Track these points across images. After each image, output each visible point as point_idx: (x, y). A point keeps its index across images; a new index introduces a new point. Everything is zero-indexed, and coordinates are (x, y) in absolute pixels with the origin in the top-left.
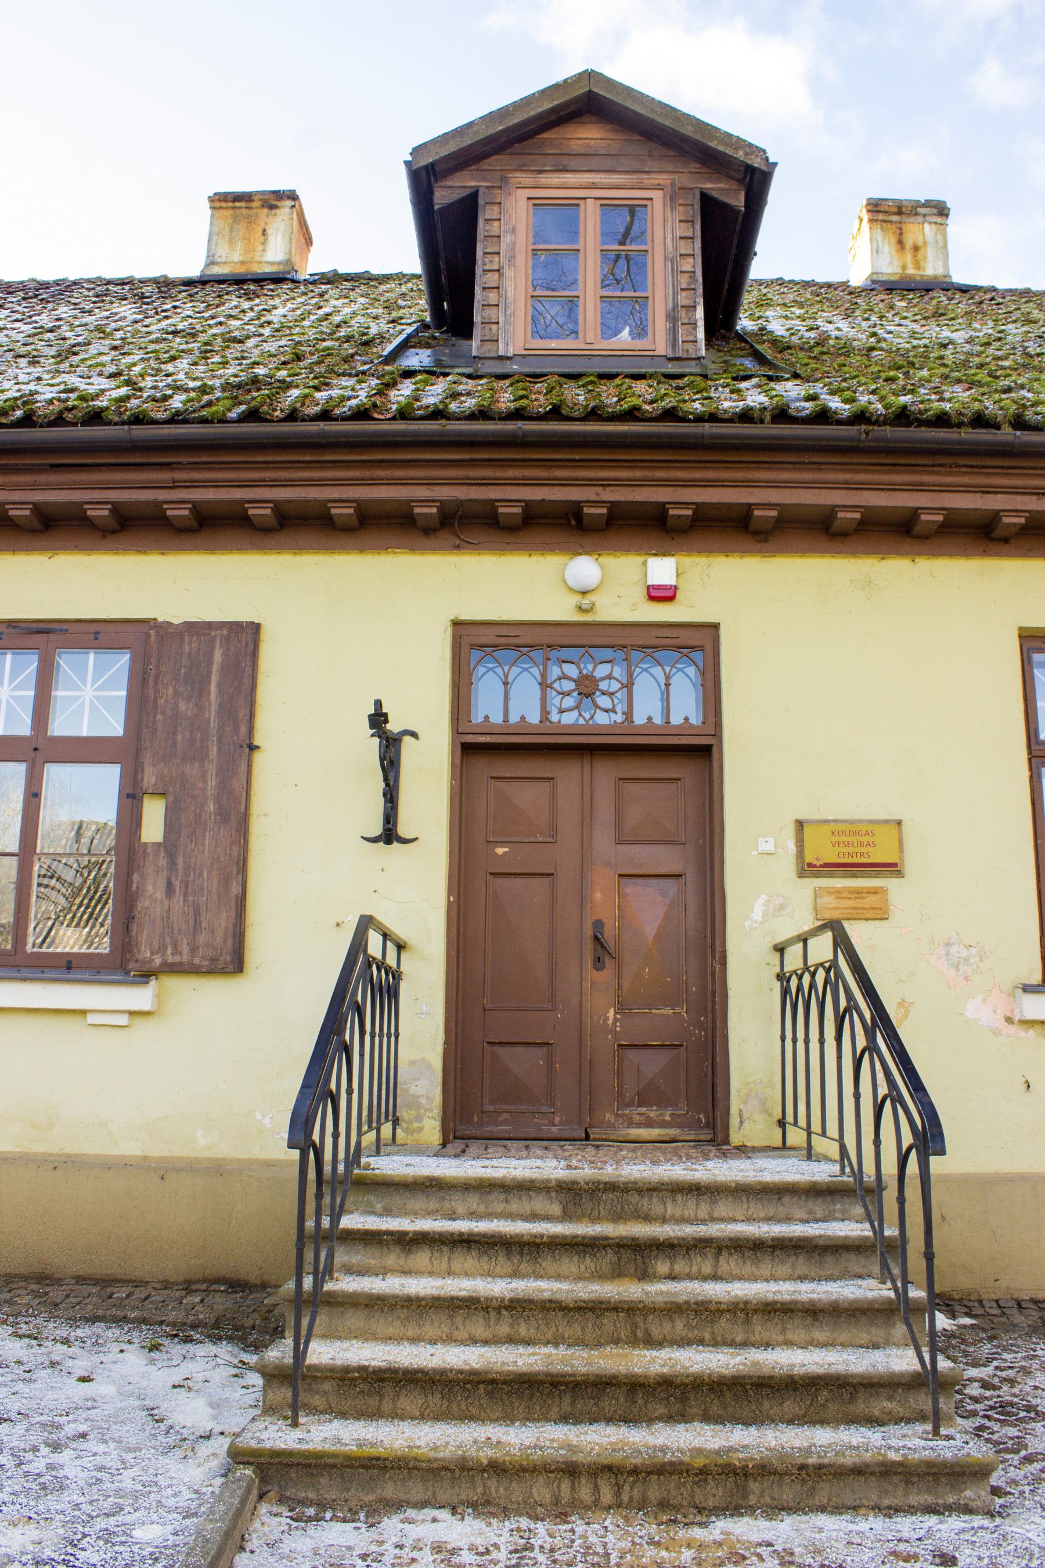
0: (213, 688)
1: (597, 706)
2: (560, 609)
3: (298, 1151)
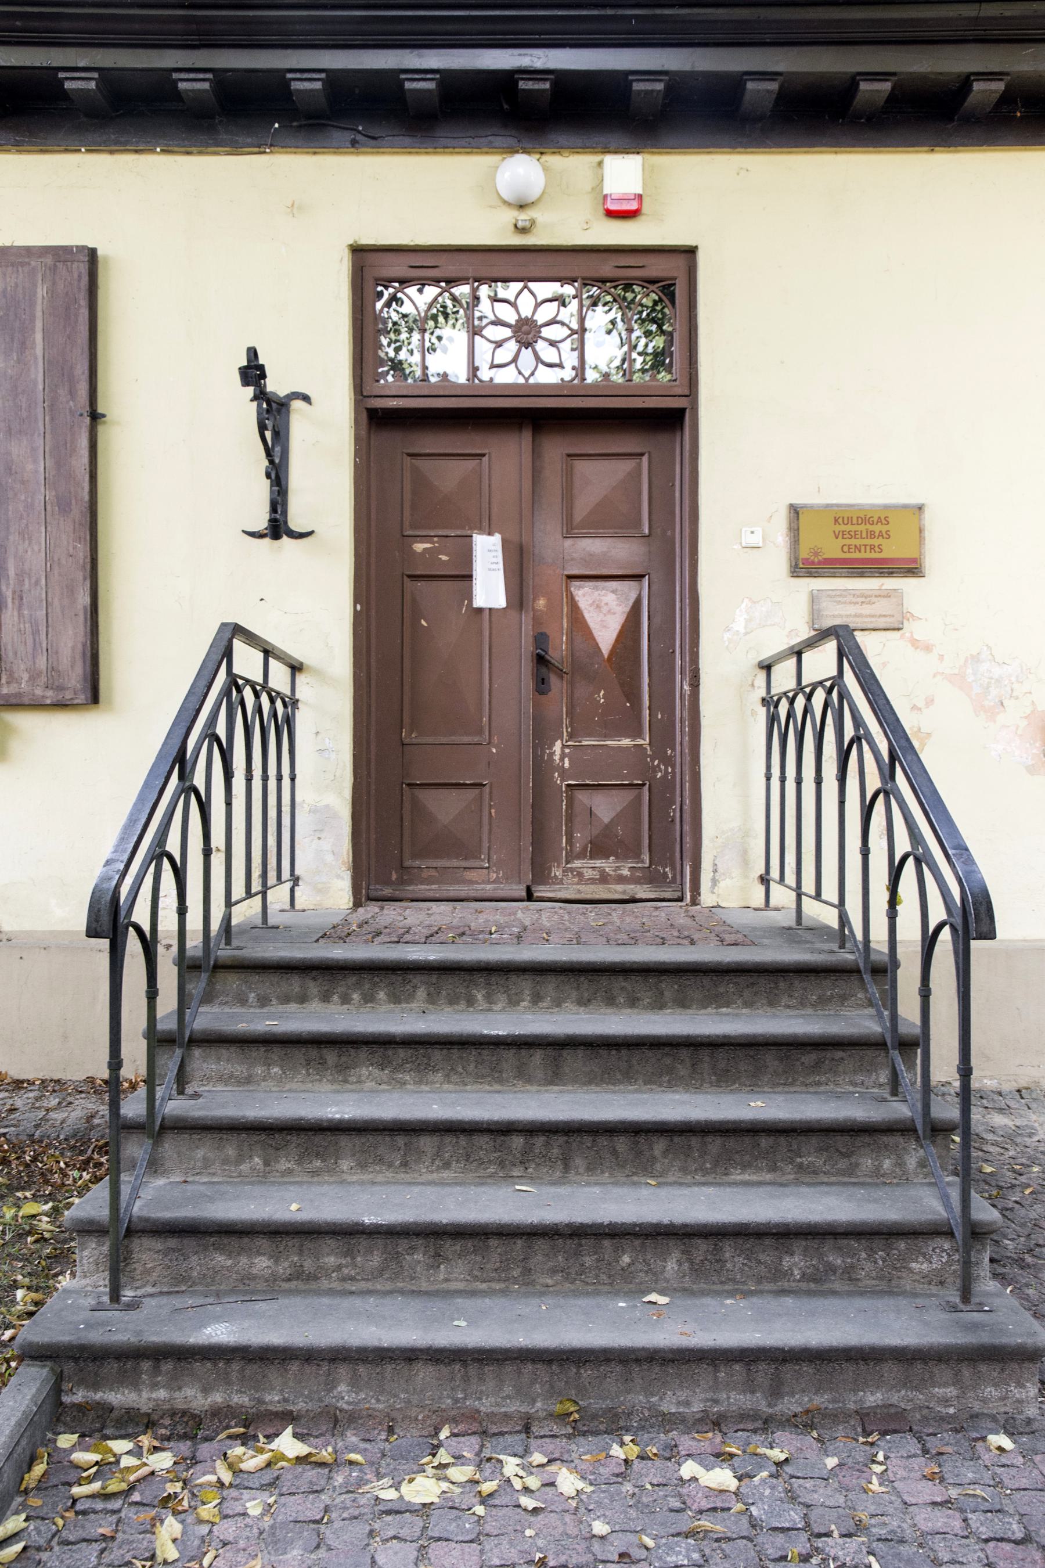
0: (39, 337)
1: (538, 359)
2: (491, 229)
3: (108, 941)
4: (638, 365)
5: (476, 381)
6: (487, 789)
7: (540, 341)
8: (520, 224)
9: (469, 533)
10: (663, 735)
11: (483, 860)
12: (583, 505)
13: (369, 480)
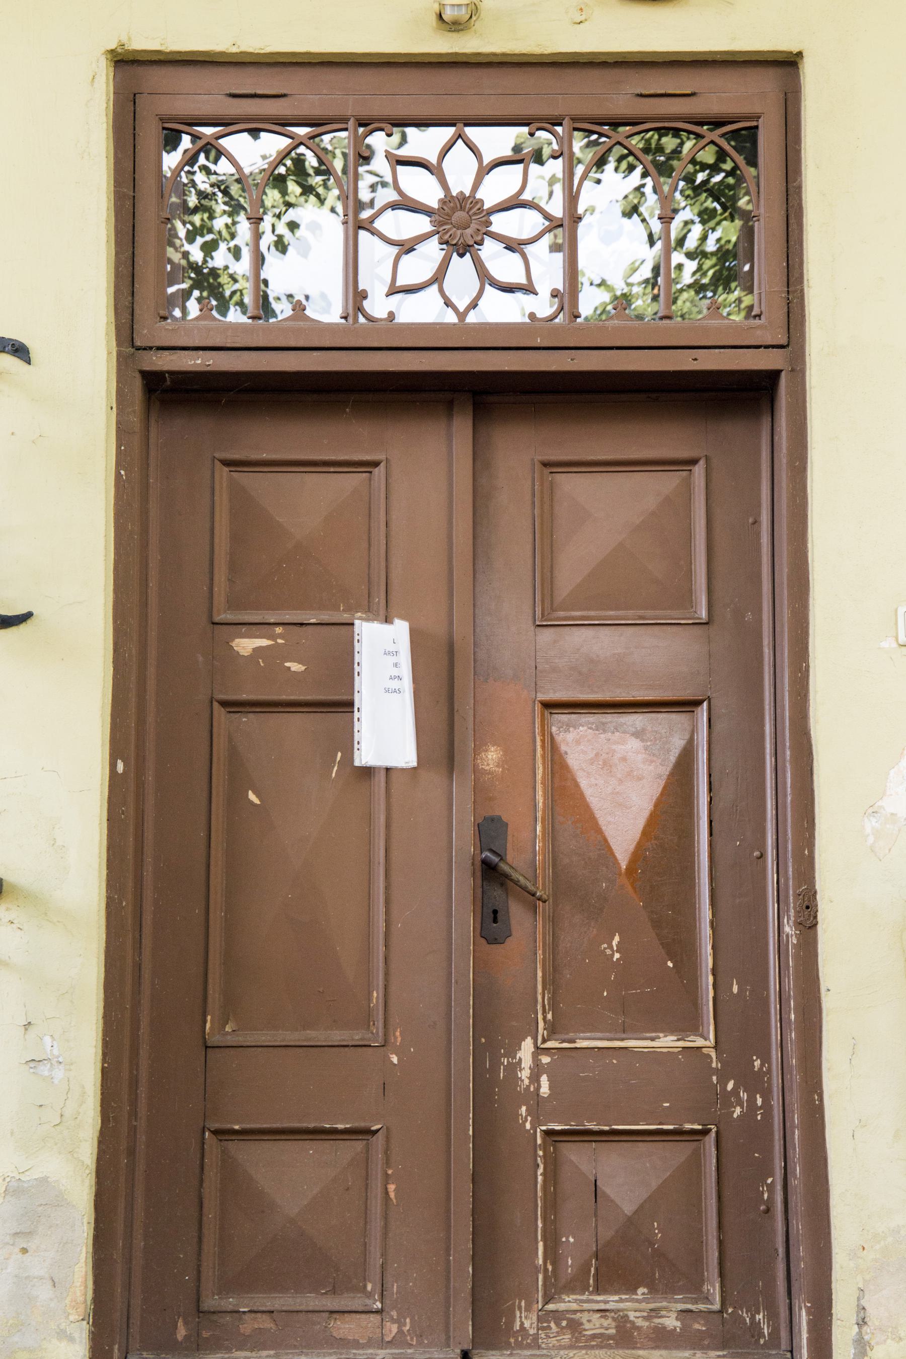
4: (687, 278)
5: (362, 320)
6: (379, 1141)
7: (488, 241)
8: (448, 15)
9: (345, 617)
10: (744, 1031)
11: (369, 1295)
12: (576, 562)
13: (144, 512)
